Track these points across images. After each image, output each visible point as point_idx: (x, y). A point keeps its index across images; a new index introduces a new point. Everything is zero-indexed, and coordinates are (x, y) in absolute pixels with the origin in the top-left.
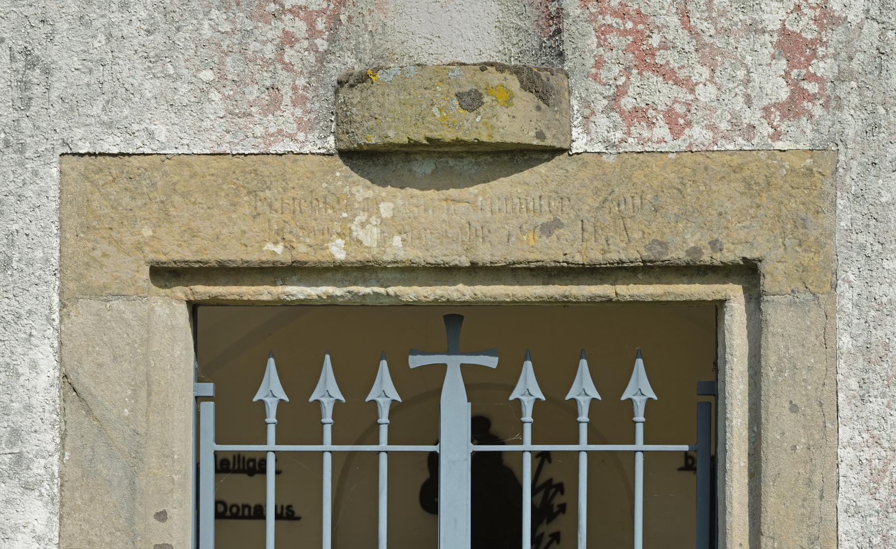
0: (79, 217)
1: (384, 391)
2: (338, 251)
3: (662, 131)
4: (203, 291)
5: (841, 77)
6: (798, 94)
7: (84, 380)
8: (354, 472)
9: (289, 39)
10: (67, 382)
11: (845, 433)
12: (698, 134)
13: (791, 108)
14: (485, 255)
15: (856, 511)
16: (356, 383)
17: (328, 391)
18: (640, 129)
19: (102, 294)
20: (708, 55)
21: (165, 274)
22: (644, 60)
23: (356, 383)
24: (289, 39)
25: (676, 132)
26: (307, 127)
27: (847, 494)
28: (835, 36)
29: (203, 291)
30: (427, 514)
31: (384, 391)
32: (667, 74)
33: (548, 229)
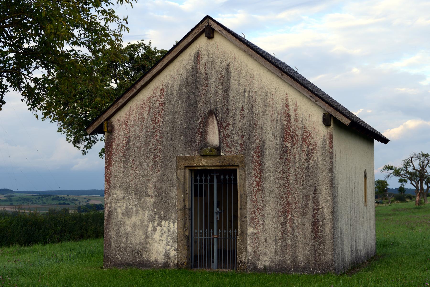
0: (178, 162)
1: (209, 178)
2: (201, 165)
3: (229, 153)
4: (190, 168)
5: (246, 147)
6: (242, 149)
7: (179, 177)
8: (206, 186)
9: (196, 145)
10: (177, 177)
11: (247, 182)
12: (232, 153)
13: (241, 150)
14: (214, 165)
15: (248, 189)
16: (206, 177)
17: (227, 177)
18: (227, 153)
19: (180, 169)
20: (233, 145)
21: (186, 167)
22: (227, 146)
23: (206, 177)
24: (196, 145)
25: (231, 153)
26: (198, 153)
27: (247, 188)
28: (245, 143)
29: (190, 168)
30: (6, 188)
31: (209, 178)
32: (230, 147)
33: (219, 162)
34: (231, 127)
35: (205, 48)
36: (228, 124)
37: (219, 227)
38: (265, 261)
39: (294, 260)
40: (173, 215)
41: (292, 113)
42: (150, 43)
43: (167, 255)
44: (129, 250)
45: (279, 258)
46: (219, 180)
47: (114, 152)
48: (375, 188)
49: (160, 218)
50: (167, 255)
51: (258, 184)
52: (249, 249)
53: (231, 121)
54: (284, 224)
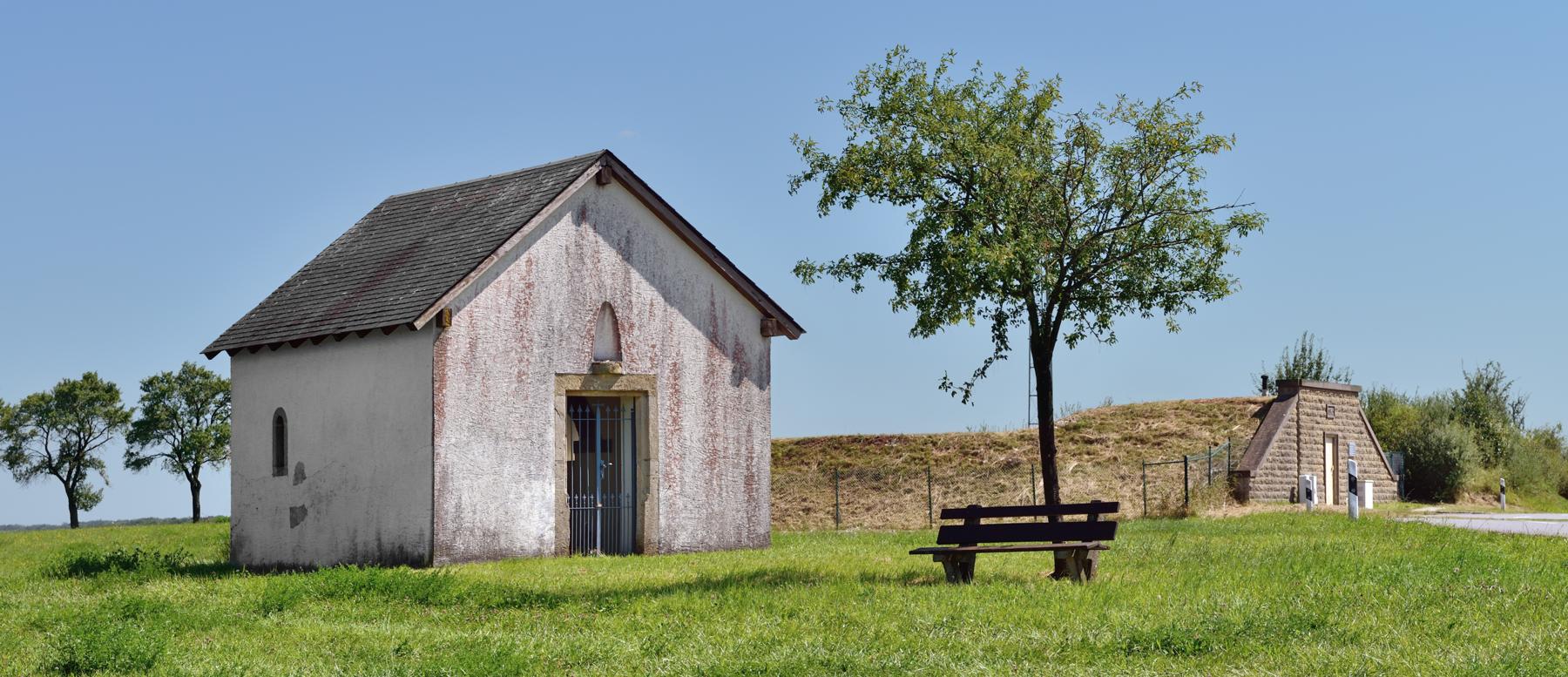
34: (636, 332)
35: (592, 199)
36: (632, 326)
37: (604, 491)
38: (683, 539)
39: (721, 536)
40: (550, 472)
41: (719, 314)
42: (1560, 427)
43: (540, 538)
44: (478, 533)
45: (700, 534)
46: (603, 415)
47: (449, 362)
48: (43, 397)
49: (529, 476)
50: (540, 538)
51: (675, 420)
52: (663, 521)
53: (635, 319)
54: (709, 482)
